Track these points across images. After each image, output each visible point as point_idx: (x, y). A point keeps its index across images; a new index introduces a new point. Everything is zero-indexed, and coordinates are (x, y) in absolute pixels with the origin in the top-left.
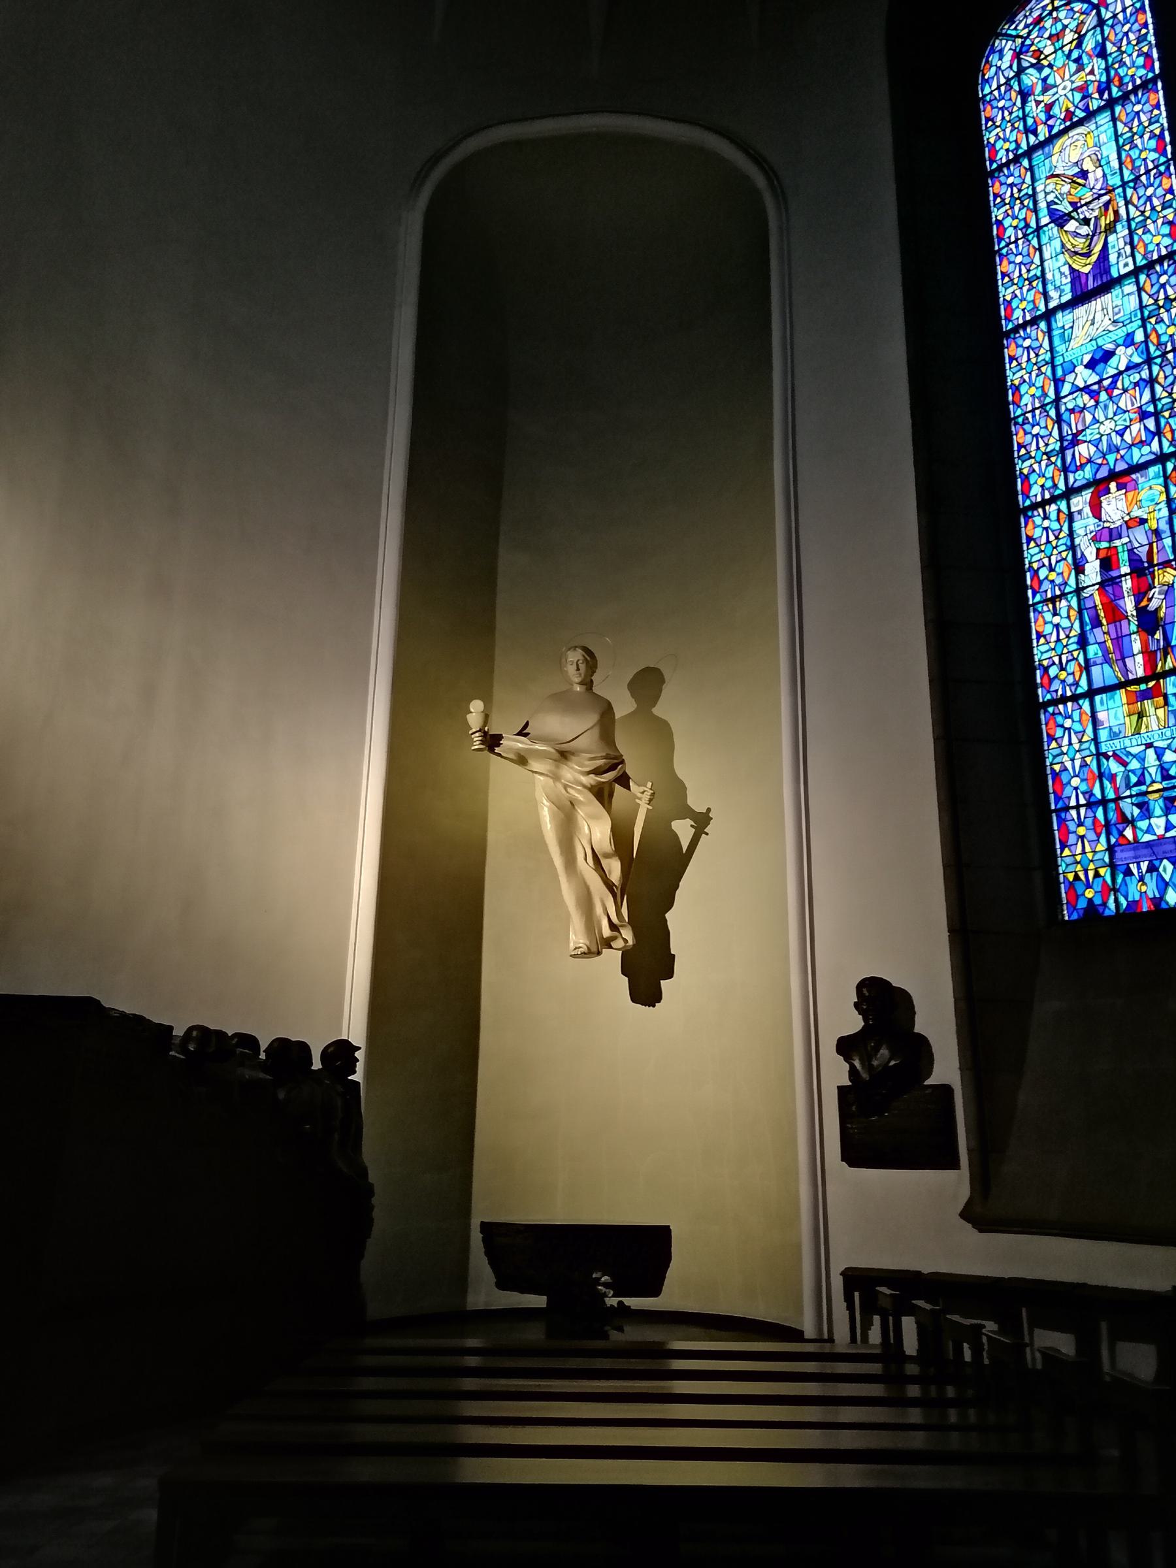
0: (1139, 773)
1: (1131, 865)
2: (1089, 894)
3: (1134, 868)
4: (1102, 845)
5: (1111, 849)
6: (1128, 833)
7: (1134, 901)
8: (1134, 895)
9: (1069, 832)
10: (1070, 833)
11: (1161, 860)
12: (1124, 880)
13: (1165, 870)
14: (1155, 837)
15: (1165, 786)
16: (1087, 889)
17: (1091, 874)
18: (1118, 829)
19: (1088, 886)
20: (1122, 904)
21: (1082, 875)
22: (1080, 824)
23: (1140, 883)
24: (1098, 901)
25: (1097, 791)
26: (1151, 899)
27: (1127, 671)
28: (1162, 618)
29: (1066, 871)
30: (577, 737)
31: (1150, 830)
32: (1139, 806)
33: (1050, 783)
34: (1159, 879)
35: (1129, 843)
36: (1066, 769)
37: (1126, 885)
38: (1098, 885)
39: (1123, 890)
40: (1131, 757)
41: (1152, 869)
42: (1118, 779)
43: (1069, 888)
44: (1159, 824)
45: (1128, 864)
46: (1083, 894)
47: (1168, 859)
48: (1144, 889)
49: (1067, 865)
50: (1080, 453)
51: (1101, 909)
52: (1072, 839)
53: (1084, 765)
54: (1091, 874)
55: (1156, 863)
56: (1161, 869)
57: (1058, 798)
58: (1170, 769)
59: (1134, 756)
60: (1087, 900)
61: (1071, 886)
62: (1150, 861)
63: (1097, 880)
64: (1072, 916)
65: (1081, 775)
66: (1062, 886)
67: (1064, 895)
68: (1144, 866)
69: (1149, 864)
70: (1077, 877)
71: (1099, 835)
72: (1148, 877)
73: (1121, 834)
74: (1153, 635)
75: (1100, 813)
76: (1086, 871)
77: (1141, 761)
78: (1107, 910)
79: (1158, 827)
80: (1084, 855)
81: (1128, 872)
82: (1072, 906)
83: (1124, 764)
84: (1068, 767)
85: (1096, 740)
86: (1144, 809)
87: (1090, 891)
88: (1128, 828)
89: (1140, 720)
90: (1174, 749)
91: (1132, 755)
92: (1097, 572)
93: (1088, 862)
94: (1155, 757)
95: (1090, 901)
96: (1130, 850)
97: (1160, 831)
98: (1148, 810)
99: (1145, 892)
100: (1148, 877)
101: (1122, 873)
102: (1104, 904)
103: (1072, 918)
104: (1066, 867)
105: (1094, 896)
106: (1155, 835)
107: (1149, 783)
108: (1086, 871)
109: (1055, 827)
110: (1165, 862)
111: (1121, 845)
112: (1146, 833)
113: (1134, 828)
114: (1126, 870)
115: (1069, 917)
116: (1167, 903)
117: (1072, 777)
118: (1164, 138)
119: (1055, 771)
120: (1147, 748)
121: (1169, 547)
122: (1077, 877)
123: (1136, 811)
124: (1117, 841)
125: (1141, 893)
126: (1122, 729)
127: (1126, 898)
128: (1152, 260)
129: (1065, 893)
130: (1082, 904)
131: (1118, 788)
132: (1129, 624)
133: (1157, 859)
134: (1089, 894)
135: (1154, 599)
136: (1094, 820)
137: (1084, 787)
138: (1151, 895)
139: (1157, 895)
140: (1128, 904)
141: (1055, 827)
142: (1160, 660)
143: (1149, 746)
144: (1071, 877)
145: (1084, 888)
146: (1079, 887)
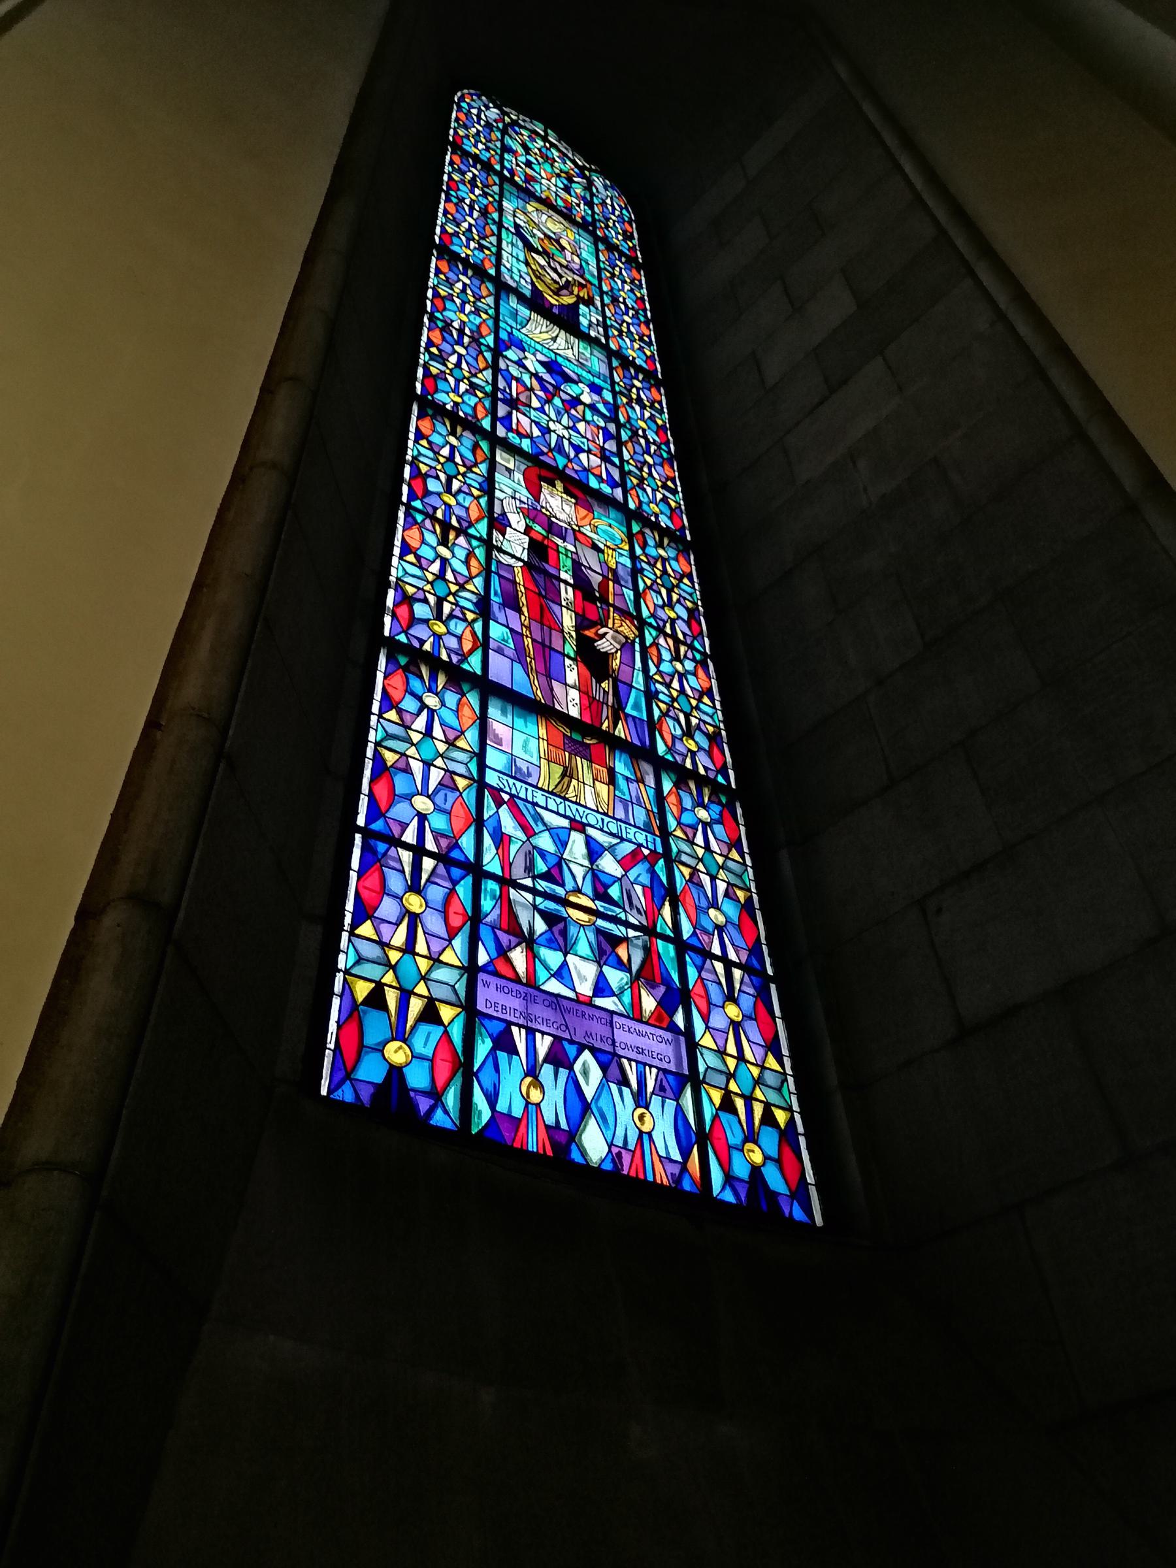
0: (552, 861)
1: (515, 1029)
2: (396, 1053)
3: (519, 1038)
4: (455, 954)
5: (471, 970)
6: (518, 957)
7: (509, 1117)
8: (511, 1101)
9: (383, 890)
10: (385, 893)
11: (581, 1049)
12: (492, 1051)
13: (585, 1073)
14: (571, 994)
15: (601, 909)
16: (393, 1039)
17: (416, 1006)
18: (497, 940)
19: (400, 1034)
20: (480, 1112)
21: (392, 998)
22: (415, 887)
23: (529, 1079)
24: (417, 1078)
25: (467, 842)
26: (547, 1127)
27: (553, 697)
28: (614, 671)
29: (353, 971)
30: (665, 1143)
31: (561, 974)
32: (547, 916)
33: (367, 773)
34: (571, 1086)
35: (517, 980)
36: (408, 770)
37: (497, 1069)
38: (426, 1039)
39: (487, 1077)
40: (541, 827)
41: (558, 1058)
42: (514, 848)
43: (350, 1016)
44: (583, 972)
45: (509, 1024)
46: (380, 1049)
47: (595, 1052)
48: (535, 1096)
49: (360, 960)
50: (517, 418)
51: (424, 1104)
52: (388, 909)
53: (448, 784)
54: (416, 1006)
55: (571, 1050)
56: (577, 1067)
57: (375, 812)
58: (609, 886)
59: (549, 829)
60: (386, 1067)
61: (353, 1012)
62: (557, 1040)
63: (424, 1028)
64: (336, 1094)
65: (439, 799)
66: (336, 1002)
67: (333, 1027)
68: (543, 1044)
69: (553, 1044)
70: (376, 999)
71: (452, 933)
72: (547, 1071)
73: (503, 952)
74: (599, 682)
75: (464, 890)
76: (405, 995)
77: (560, 846)
78: (439, 1113)
79: (583, 979)
80: (407, 957)
81: (504, 1042)
82: (344, 1072)
83: (529, 832)
84: (556, 991)
85: (481, 756)
86: (556, 929)
87: (400, 1048)
88: (519, 949)
89: (566, 779)
90: (619, 858)
91: (544, 824)
92: (524, 549)
93: (416, 977)
94: (584, 851)
95: (396, 1073)
96: (518, 995)
97: (585, 988)
98: (564, 933)
99: (538, 1105)
100: (547, 1071)
101: (491, 1036)
102: (436, 1095)
103: (338, 1095)
104: (357, 963)
105: (407, 1065)
106: (574, 990)
107: (465, 568)
108: (405, 995)
109: (355, 863)
110: (587, 1055)
111: (496, 974)
112: (553, 976)
113: (532, 957)
114: (501, 1032)
115: (330, 1091)
116: (583, 1153)
117: (418, 794)
118: (642, 400)
119: (384, 761)
120: (572, 828)
121: (630, 600)
122: (376, 999)
123: (540, 926)
124: (491, 961)
125: (528, 1103)
126: (534, 770)
127: (492, 1100)
128: (631, 569)
129: (338, 1022)
130: (371, 1071)
131: (511, 864)
132: (564, 643)
133: (571, 1042)
134: (396, 1053)
135: (604, 640)
136: (449, 894)
137: (438, 822)
138: (550, 1119)
139: (564, 1125)
140: (492, 1118)
141: (355, 863)
142: (607, 718)
143: (578, 826)
144: (362, 990)
145: (389, 1035)
146: (375, 1027)
